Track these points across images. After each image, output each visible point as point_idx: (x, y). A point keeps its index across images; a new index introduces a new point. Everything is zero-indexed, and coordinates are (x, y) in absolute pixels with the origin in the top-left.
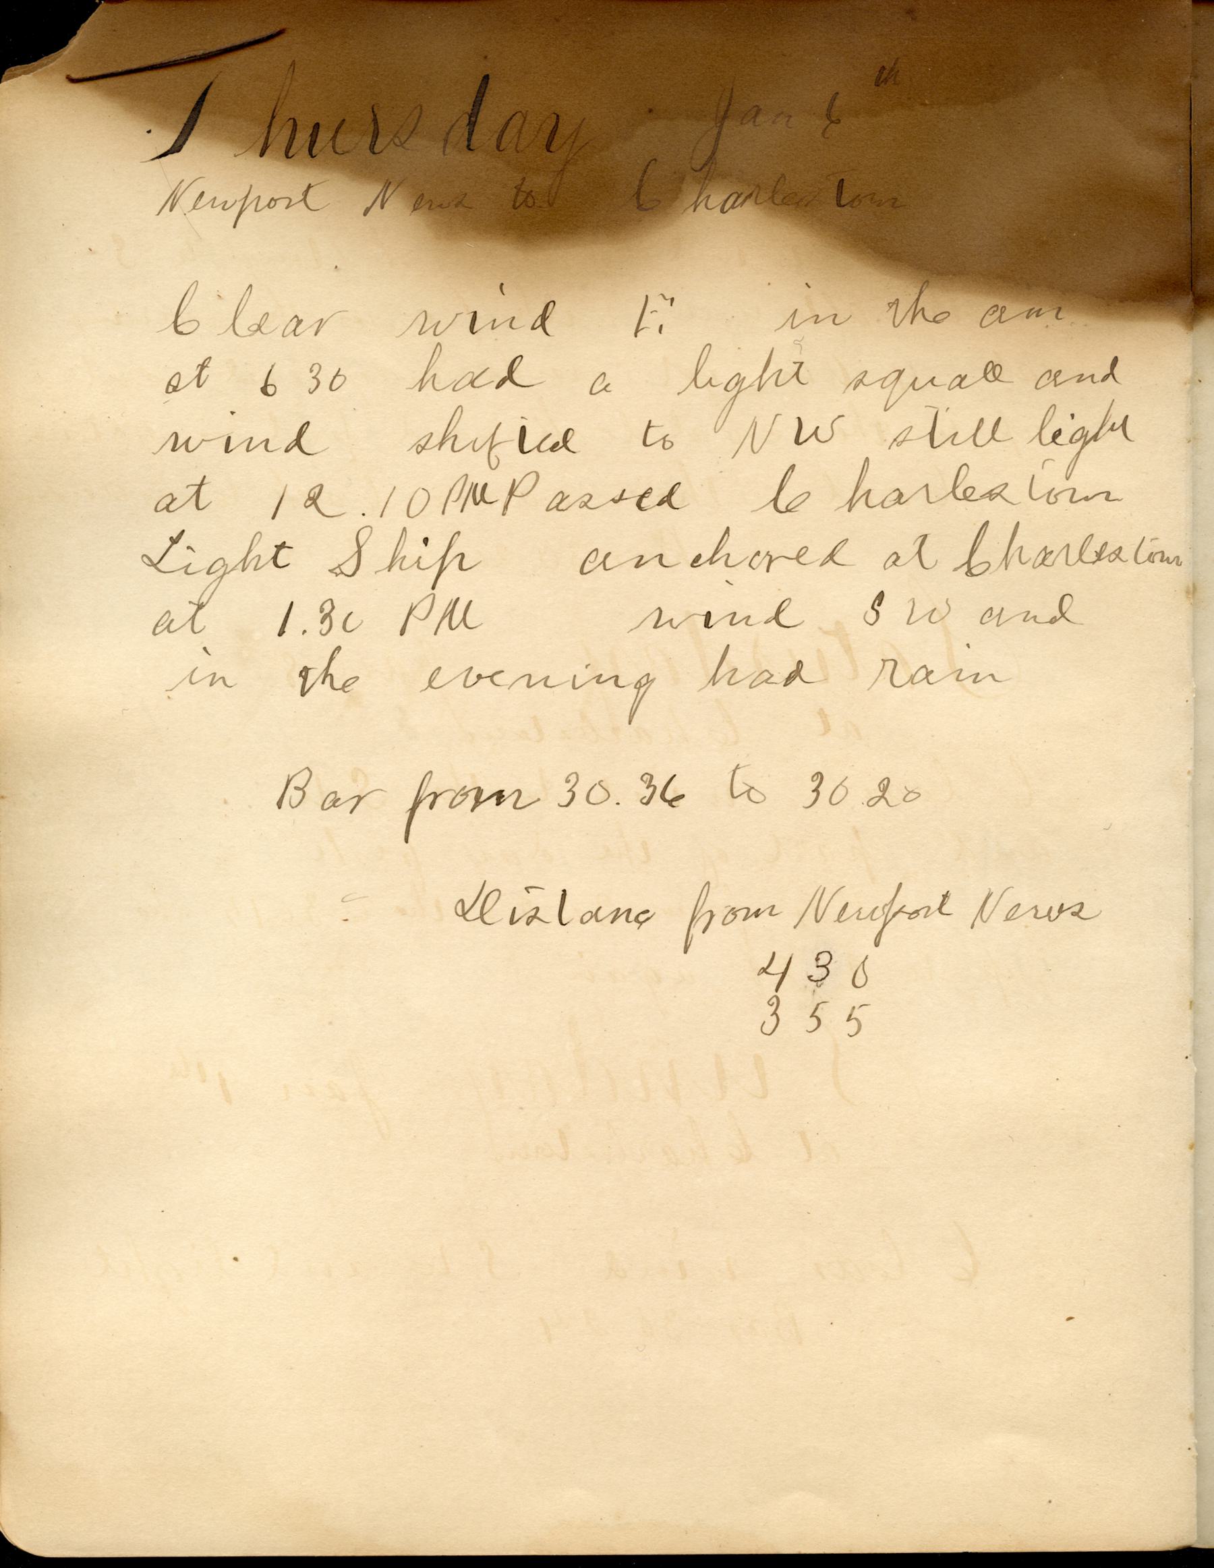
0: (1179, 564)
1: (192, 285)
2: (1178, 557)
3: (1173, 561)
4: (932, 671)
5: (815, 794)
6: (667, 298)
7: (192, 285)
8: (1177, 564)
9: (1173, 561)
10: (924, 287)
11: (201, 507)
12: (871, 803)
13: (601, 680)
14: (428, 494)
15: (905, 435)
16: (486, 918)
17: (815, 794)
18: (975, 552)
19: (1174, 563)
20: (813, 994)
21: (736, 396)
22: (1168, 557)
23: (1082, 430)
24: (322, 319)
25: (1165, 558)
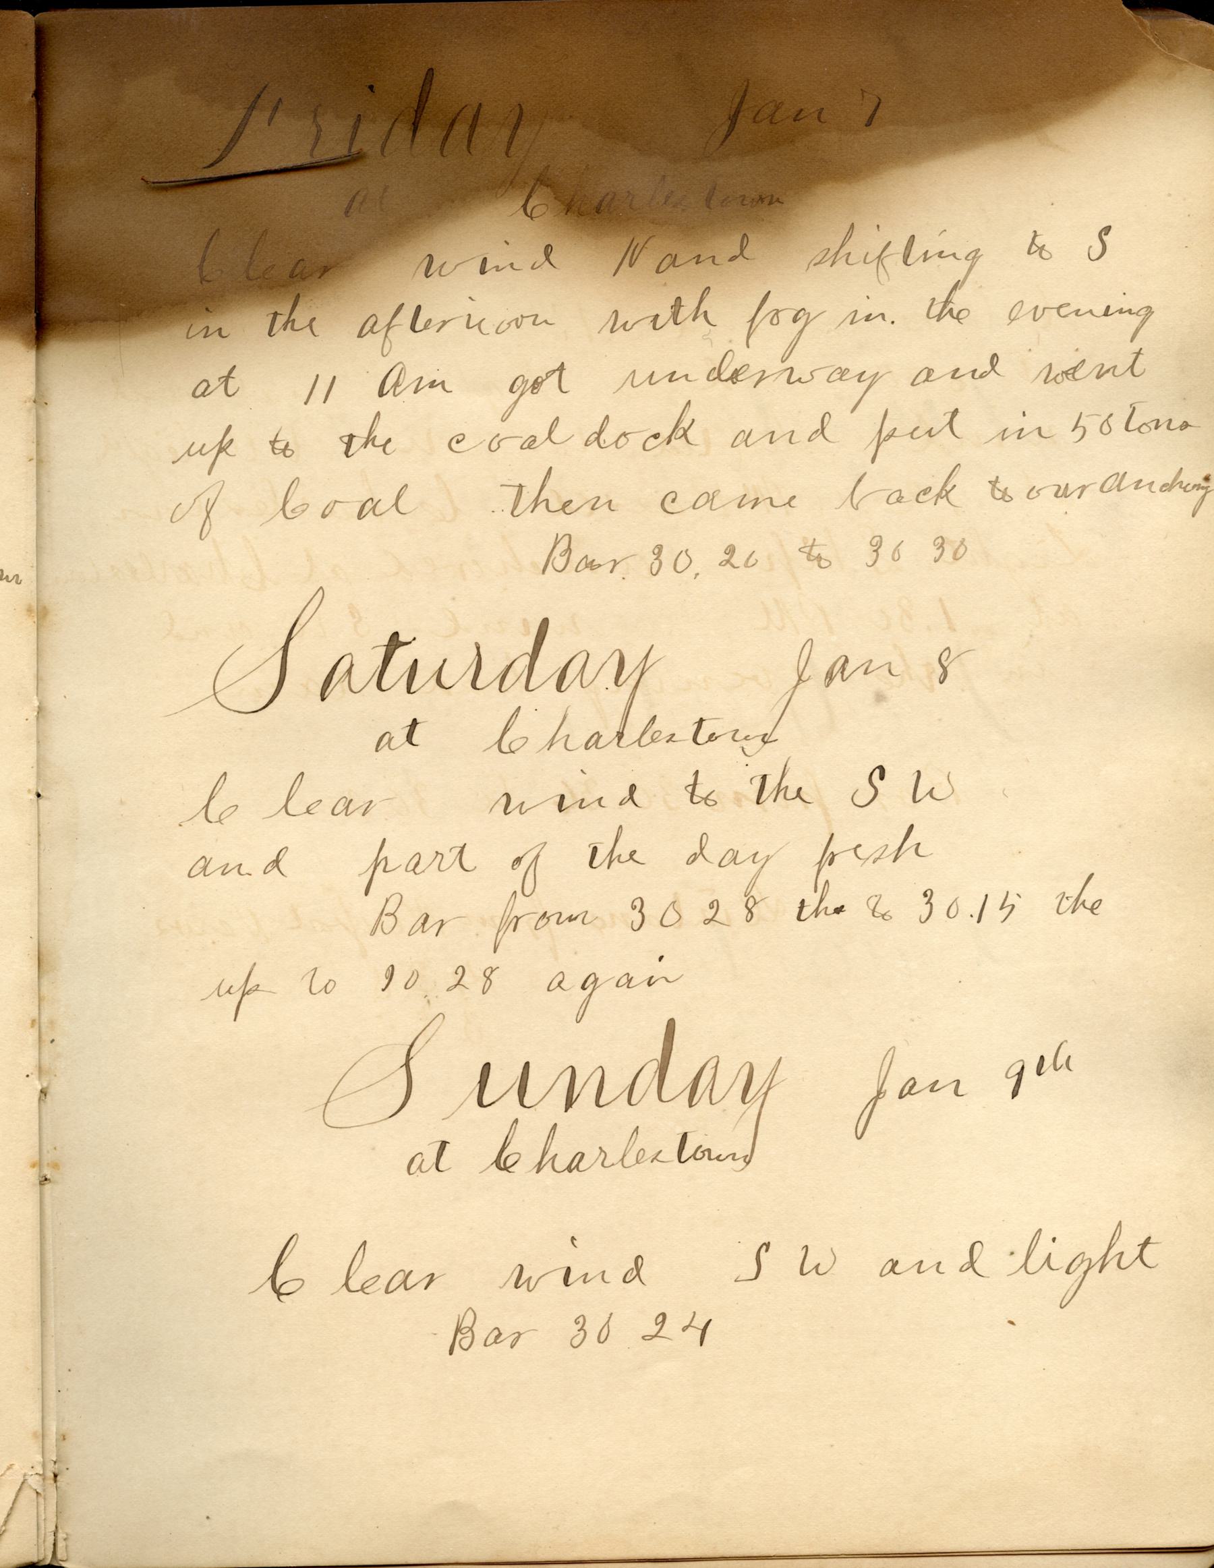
0: (18, 583)
2: (17, 575)
3: (13, 579)
5: (929, 905)
8: (17, 583)
9: (13, 579)
10: (537, 187)
11: (530, 688)
13: (764, 1247)
17: (929, 905)
18: (603, 431)
19: (14, 581)
20: (55, 1481)
21: (1109, 1248)
22: (7, 576)
23: (1116, 476)
24: (852, 323)
25: (4, 577)
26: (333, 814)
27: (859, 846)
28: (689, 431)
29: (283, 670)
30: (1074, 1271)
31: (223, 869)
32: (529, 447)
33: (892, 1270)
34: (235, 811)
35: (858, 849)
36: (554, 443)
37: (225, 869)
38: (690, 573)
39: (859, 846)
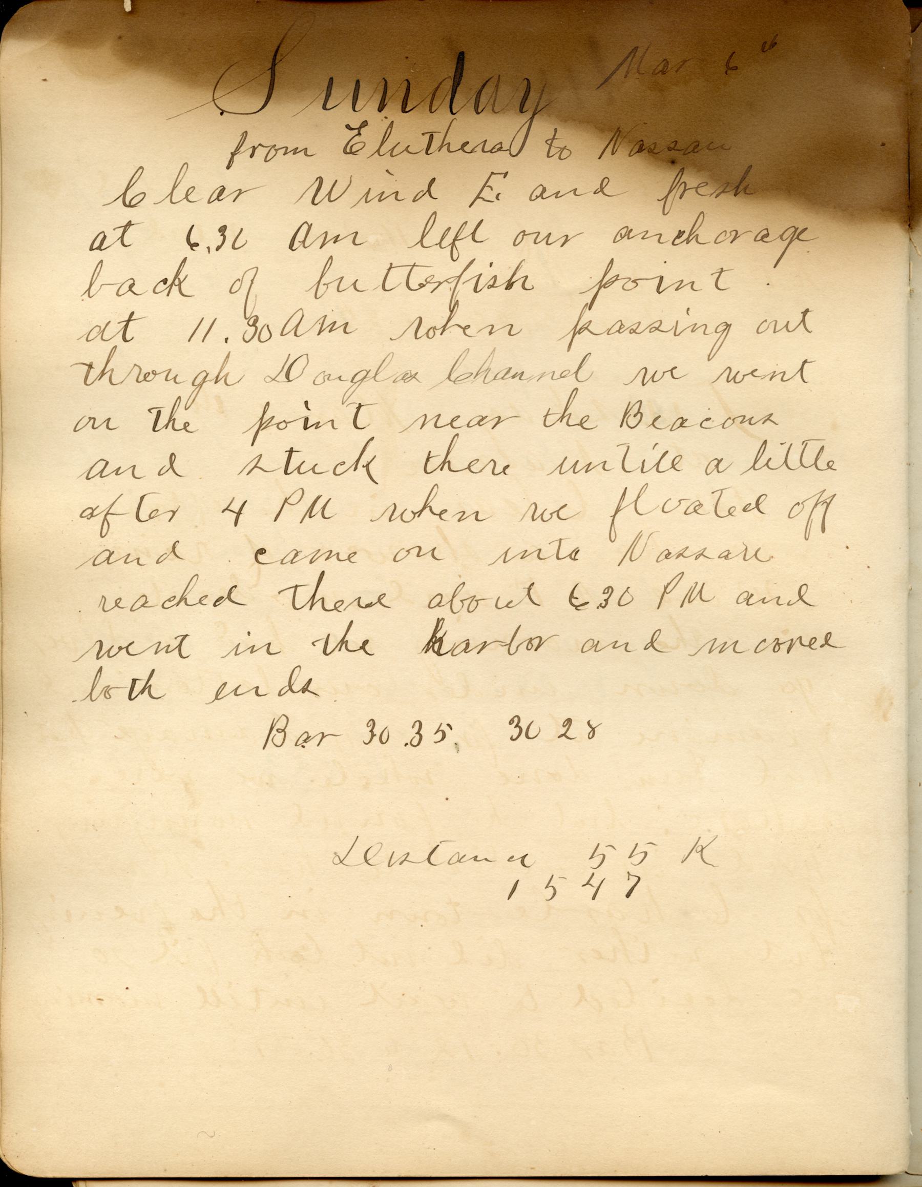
1: (453, 277)
4: (687, 420)
6: (260, 147)
7: (453, 277)
12: (814, 640)
14: (294, 505)
15: (318, 554)
16: (189, 198)
26: (395, 560)
27: (675, 368)
28: (228, 511)
29: (429, 144)
30: (623, 332)
31: (692, 327)
32: (762, 239)
33: (681, 425)
34: (186, 405)
35: (674, 371)
36: (408, 522)
37: (694, 328)
38: (326, 374)
39: (675, 368)
